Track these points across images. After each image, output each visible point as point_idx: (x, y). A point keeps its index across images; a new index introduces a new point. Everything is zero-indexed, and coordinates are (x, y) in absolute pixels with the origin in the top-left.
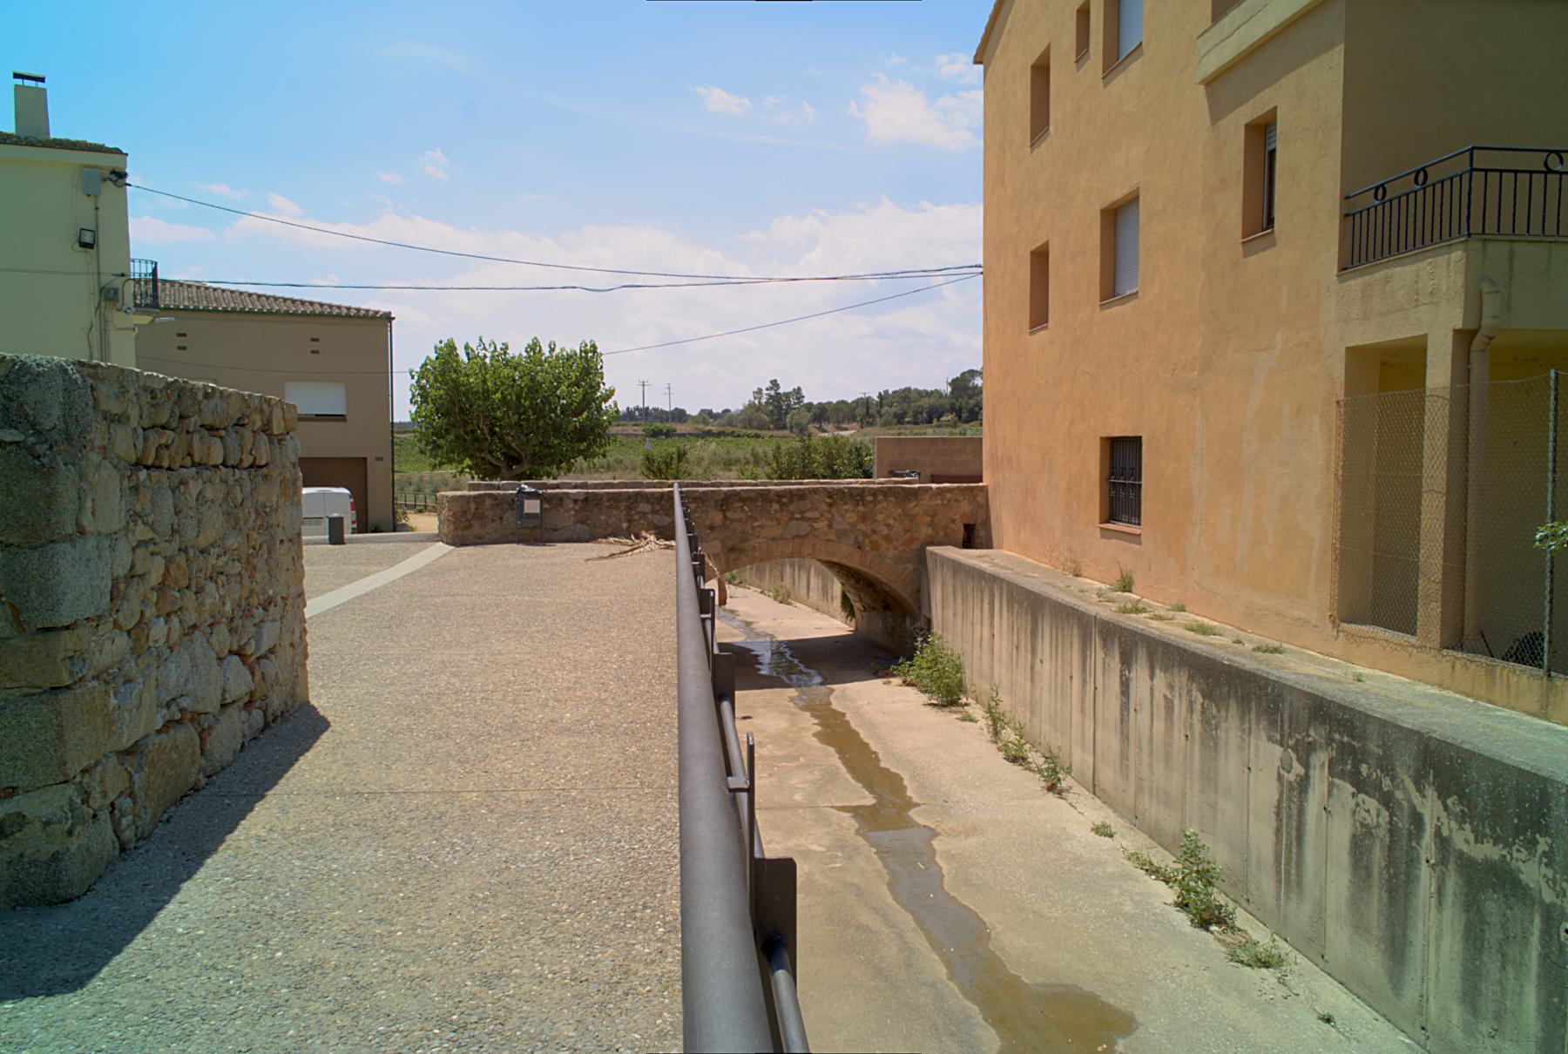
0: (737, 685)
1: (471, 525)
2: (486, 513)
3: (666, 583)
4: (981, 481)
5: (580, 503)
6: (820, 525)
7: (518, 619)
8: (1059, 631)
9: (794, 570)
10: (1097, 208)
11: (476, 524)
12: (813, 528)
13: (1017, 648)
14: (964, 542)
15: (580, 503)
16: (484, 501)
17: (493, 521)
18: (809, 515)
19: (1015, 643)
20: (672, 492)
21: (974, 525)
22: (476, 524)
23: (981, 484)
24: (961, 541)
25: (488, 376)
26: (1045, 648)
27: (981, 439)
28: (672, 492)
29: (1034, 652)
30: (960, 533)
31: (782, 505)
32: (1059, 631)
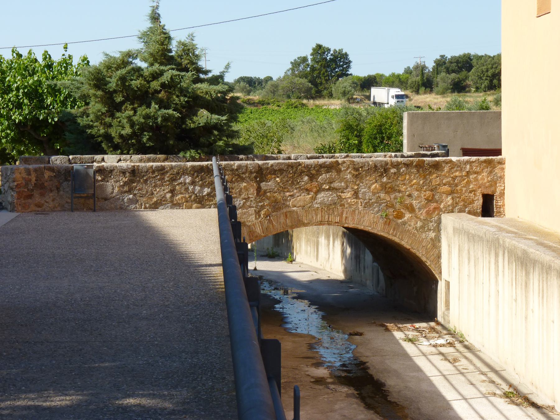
0: (249, 260)
1: (32, 195)
2: (46, 184)
3: (207, 241)
4: (501, 154)
5: (128, 174)
6: (348, 194)
7: (92, 264)
8: (545, 283)
9: (329, 240)
10: (335, 48)
11: (36, 194)
12: (340, 197)
13: (516, 301)
14: (483, 211)
15: (128, 174)
16: (43, 174)
17: (51, 191)
18: (336, 185)
19: (514, 297)
20: (211, 165)
21: (493, 196)
22: (36, 194)
23: (499, 157)
24: (479, 210)
25: (154, 106)
26: (534, 297)
27: (500, 113)
28: (211, 165)
29: (527, 304)
30: (479, 202)
31: (312, 178)
32: (545, 283)
